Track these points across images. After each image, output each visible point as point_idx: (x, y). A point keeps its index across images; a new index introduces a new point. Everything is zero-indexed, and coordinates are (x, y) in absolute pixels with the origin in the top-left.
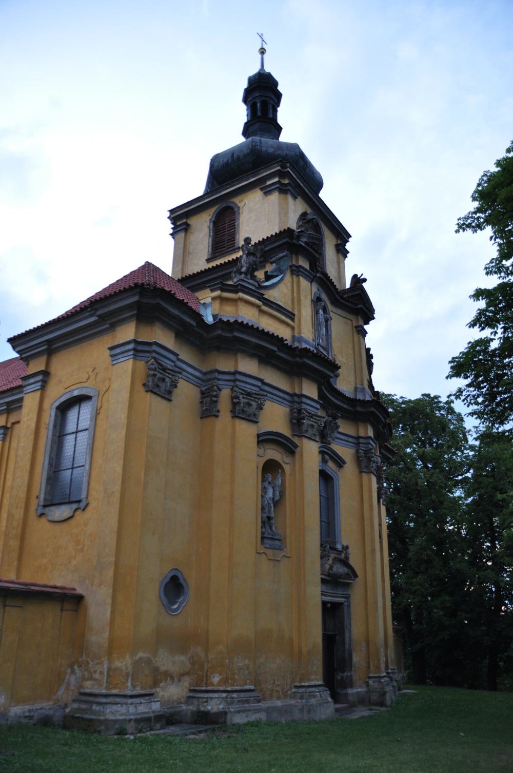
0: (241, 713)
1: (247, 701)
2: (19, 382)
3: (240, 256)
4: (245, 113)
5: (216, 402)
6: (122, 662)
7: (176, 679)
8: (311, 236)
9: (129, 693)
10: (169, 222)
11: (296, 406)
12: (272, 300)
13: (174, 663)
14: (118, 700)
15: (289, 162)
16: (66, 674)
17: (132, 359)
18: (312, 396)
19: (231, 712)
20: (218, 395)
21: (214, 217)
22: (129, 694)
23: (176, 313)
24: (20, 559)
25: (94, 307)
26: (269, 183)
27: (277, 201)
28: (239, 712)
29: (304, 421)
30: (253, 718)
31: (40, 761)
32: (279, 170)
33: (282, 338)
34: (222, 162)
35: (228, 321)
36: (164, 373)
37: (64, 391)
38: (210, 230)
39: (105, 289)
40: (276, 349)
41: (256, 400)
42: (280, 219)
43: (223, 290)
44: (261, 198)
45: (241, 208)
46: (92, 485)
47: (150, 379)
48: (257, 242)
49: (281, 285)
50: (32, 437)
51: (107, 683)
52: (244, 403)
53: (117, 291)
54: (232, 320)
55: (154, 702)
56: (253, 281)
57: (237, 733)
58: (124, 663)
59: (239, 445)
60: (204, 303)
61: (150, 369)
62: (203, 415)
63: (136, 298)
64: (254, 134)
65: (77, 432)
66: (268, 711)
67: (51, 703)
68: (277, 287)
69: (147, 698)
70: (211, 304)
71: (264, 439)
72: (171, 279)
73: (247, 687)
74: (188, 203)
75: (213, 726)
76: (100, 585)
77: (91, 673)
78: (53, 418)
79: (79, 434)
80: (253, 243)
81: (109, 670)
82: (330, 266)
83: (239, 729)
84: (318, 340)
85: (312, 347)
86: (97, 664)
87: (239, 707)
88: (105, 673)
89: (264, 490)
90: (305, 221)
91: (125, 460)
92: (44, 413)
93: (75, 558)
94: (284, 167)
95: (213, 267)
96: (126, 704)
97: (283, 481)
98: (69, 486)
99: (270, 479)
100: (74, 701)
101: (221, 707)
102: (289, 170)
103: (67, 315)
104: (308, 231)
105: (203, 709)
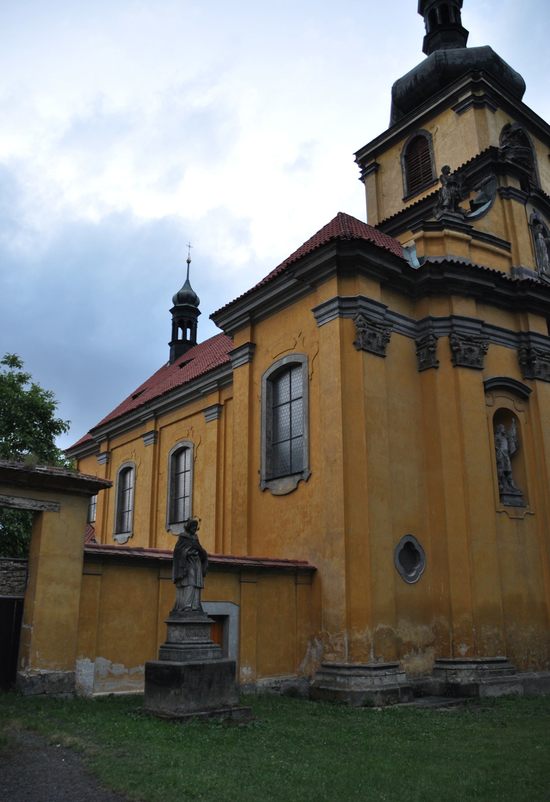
0: (495, 686)
1: (500, 673)
2: (227, 358)
3: (440, 189)
4: (423, 25)
5: (434, 352)
6: (362, 634)
7: (420, 650)
8: (519, 150)
9: (373, 665)
10: (356, 165)
11: (524, 345)
12: (482, 231)
13: (416, 633)
14: (361, 672)
15: (483, 70)
16: (307, 646)
17: (338, 318)
18: (541, 333)
19: (483, 684)
20: (434, 344)
21: (405, 150)
22: (373, 666)
23: (379, 262)
24: (249, 536)
25: (292, 270)
26: (461, 100)
27: (473, 118)
28: (492, 684)
29: (535, 362)
30: (508, 690)
31: (292, 729)
32: (471, 82)
33: (499, 272)
34: (404, 88)
35: (436, 262)
36: (373, 328)
37: (272, 361)
38: (402, 166)
39: (300, 249)
40: (493, 285)
41: (478, 345)
42: (480, 138)
43: (426, 229)
44: (454, 119)
45: (433, 134)
46: (313, 454)
47: (360, 337)
48: (457, 169)
49: (491, 214)
50: (247, 412)
51: (349, 654)
52: (464, 350)
53: (313, 248)
54: (440, 261)
55: (399, 674)
56: (458, 214)
57: (492, 707)
58: (364, 635)
59: (465, 395)
60: (407, 247)
61: (358, 326)
62: (421, 368)
63: (334, 253)
64: (437, 47)
65: (290, 402)
66: (524, 683)
67: (296, 675)
68: (486, 216)
69: (391, 670)
70: (414, 246)
71: (492, 387)
72: (367, 227)
73: (498, 658)
74: (374, 141)
75: (464, 699)
76: (332, 557)
77: (332, 645)
78: (265, 390)
79: (294, 404)
80: (452, 171)
81: (350, 642)
82: (545, 182)
83: (494, 702)
84: (541, 269)
85: (535, 277)
86: (337, 636)
87: (491, 679)
88: (346, 645)
89: (498, 443)
90: (509, 135)
91: (344, 425)
92: (256, 386)
93: (303, 531)
94: (476, 77)
95: (419, 201)
96: (371, 676)
97: (518, 430)
98: (289, 458)
99: (503, 430)
100: (318, 673)
101: (471, 679)
102: (482, 79)
103: (265, 282)
104: (513, 145)
105: (452, 681)
